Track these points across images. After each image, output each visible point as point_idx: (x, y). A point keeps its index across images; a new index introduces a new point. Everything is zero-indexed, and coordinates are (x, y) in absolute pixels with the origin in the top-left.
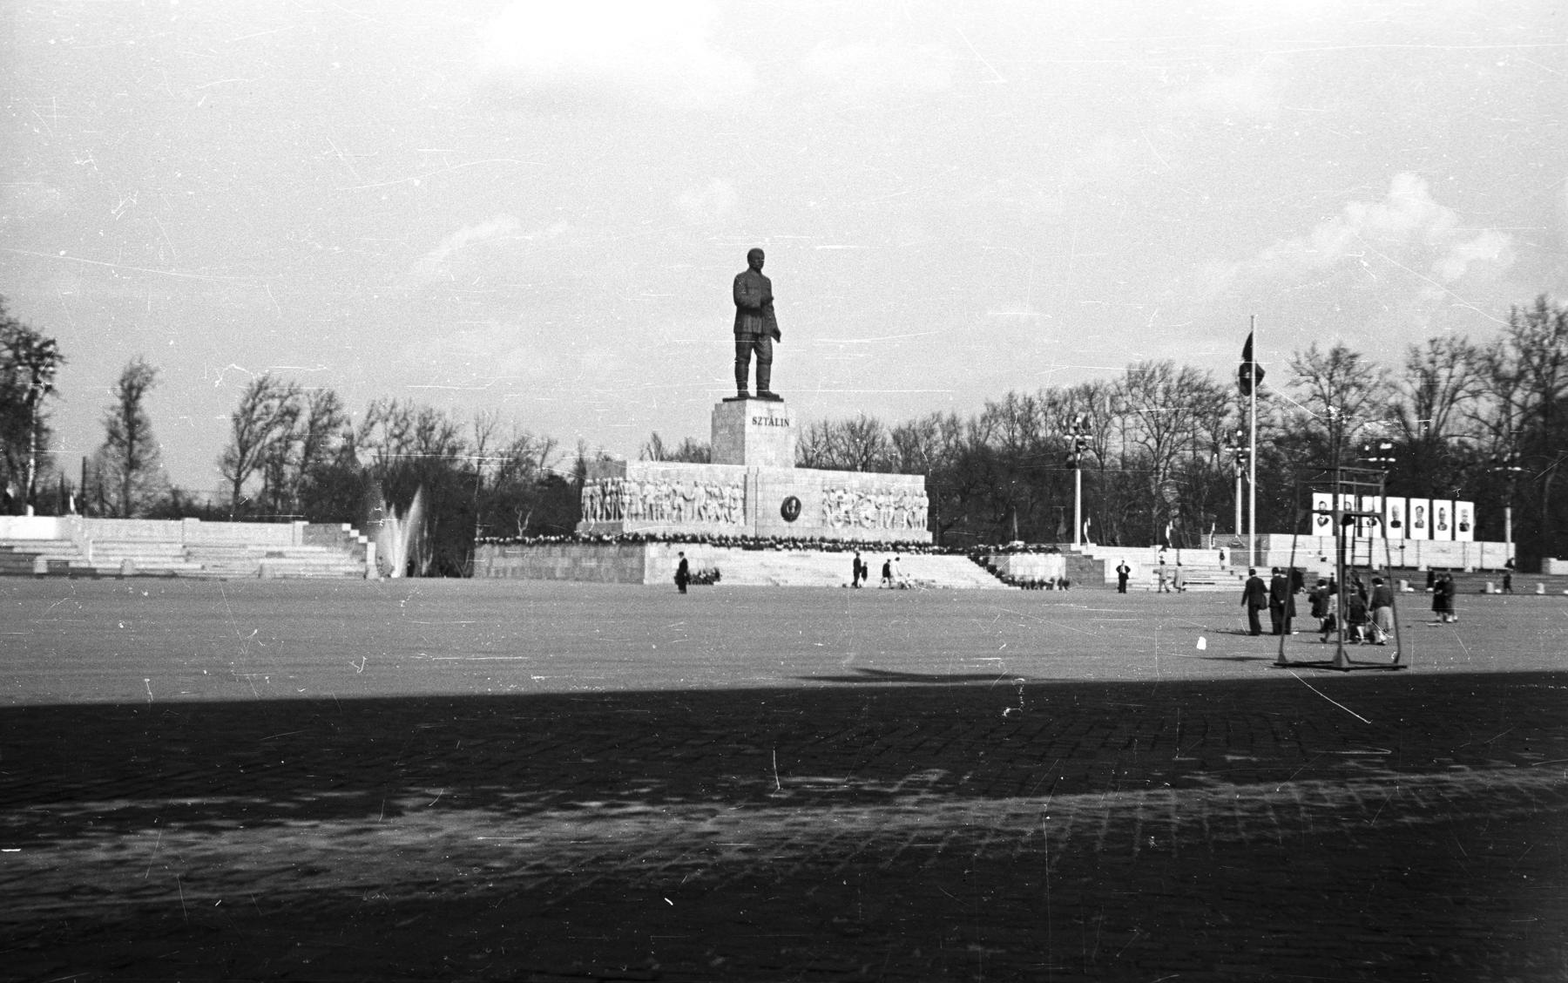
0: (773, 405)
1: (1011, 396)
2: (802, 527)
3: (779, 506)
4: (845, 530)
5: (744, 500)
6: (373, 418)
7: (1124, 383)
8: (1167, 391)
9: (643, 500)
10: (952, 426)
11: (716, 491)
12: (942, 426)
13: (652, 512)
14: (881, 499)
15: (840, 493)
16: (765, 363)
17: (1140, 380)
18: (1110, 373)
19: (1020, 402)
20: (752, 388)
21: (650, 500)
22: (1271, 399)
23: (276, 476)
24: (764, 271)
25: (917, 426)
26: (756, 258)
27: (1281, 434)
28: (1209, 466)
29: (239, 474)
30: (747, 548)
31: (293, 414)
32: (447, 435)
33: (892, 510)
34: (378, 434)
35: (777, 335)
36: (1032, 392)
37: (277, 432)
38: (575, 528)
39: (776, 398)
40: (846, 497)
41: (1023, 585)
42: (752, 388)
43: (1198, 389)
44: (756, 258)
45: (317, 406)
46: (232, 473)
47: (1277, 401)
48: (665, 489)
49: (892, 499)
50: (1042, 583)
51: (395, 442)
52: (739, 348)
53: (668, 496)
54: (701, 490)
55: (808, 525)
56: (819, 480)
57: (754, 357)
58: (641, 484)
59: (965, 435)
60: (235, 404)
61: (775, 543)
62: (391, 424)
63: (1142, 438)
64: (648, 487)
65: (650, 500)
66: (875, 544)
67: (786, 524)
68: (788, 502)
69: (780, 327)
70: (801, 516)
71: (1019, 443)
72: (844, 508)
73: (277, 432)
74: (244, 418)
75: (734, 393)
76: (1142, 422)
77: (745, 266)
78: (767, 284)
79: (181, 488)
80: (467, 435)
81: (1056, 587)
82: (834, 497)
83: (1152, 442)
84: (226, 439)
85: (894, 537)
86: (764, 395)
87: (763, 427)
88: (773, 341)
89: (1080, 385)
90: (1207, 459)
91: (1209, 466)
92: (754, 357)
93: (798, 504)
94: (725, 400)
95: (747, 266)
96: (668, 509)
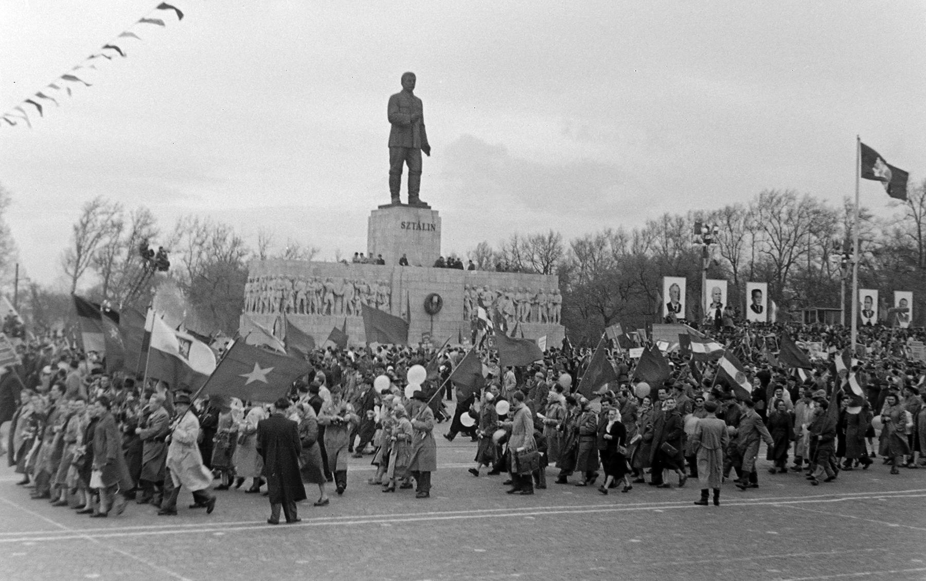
0: (421, 211)
1: (666, 216)
5: (390, 296)
6: (180, 231)
7: (756, 205)
8: (790, 214)
10: (621, 238)
11: (364, 288)
12: (611, 240)
14: (519, 296)
15: (480, 290)
17: (769, 202)
18: (744, 198)
19: (674, 221)
22: (873, 219)
23: (107, 274)
25: (593, 240)
26: (409, 80)
27: (878, 246)
28: (821, 272)
29: (76, 272)
31: (119, 226)
32: (236, 243)
33: (528, 306)
34: (185, 242)
35: (427, 150)
36: (683, 214)
37: (106, 240)
42: (404, 197)
43: (817, 212)
44: (409, 80)
45: (138, 221)
46: (71, 271)
47: (878, 221)
48: (316, 286)
49: (528, 296)
51: (197, 249)
52: (392, 161)
53: (318, 292)
54: (350, 287)
56: (460, 280)
57: (406, 169)
59: (629, 249)
60: (76, 216)
62: (194, 234)
63: (767, 249)
65: (301, 296)
68: (430, 298)
69: (430, 142)
70: (444, 310)
71: (670, 253)
73: (106, 240)
74: (82, 228)
75: (388, 200)
76: (768, 236)
77: (399, 88)
78: (417, 105)
79: (38, 283)
80: (251, 245)
82: (474, 294)
83: (776, 253)
84: (68, 243)
88: (423, 154)
89: (723, 207)
90: (819, 266)
91: (821, 272)
92: (406, 169)
93: (440, 301)
94: (380, 207)
96: (318, 303)
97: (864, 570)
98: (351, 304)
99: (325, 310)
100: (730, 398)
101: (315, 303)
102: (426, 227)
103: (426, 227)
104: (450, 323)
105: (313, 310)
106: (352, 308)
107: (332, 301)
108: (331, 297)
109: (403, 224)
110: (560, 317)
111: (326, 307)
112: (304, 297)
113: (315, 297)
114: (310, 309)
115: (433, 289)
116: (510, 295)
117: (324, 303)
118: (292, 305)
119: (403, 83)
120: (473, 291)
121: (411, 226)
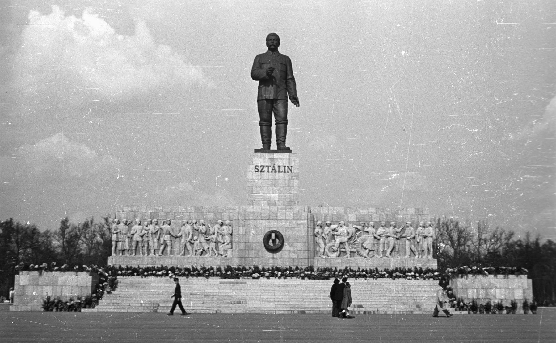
2: (281, 260)
3: (261, 238)
4: (339, 260)
9: (131, 238)
13: (137, 248)
16: (283, 122)
20: (274, 146)
21: (137, 237)
24: (280, 50)
26: (273, 41)
30: (225, 276)
38: (107, 263)
39: (288, 150)
40: (340, 230)
41: (474, 307)
42: (274, 146)
44: (273, 41)
50: (500, 307)
54: (188, 228)
55: (293, 255)
58: (128, 224)
61: (259, 272)
64: (136, 227)
65: (137, 237)
66: (371, 272)
67: (270, 255)
68: (267, 237)
72: (338, 240)
78: (286, 63)
81: (520, 311)
85: (393, 263)
86: (283, 148)
87: (265, 175)
95: (266, 49)
96: (153, 243)
97: (265, 332)
98: (188, 244)
99: (160, 251)
100: (117, 204)
101: (151, 244)
102: (282, 169)
103: (282, 169)
104: (294, 259)
105: (149, 250)
106: (189, 247)
107: (169, 243)
108: (167, 237)
109: (256, 167)
110: (431, 250)
111: (162, 247)
112: (140, 239)
113: (151, 239)
114: (145, 251)
115: (274, 225)
116: (370, 229)
117: (160, 245)
118: (127, 247)
119: (268, 44)
120: (326, 228)
121: (266, 169)
